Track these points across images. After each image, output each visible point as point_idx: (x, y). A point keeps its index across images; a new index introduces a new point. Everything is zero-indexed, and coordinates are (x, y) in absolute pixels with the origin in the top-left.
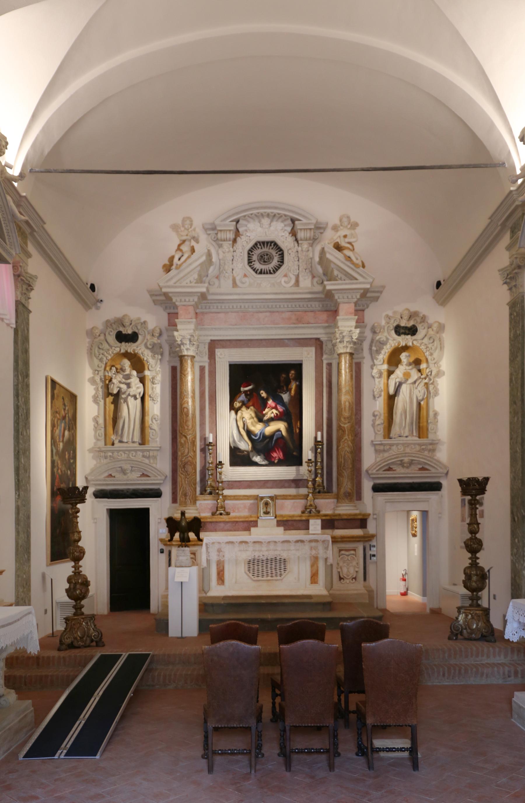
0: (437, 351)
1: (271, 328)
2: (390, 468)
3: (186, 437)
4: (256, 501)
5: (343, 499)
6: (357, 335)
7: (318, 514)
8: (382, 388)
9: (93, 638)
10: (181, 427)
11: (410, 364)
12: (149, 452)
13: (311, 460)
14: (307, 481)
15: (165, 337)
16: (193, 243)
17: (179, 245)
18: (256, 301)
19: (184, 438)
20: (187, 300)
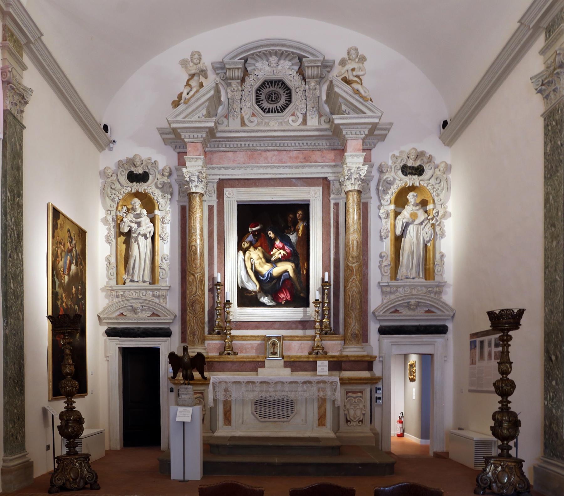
0: (444, 191)
1: (279, 166)
2: (396, 310)
3: (194, 276)
4: (263, 342)
5: (351, 341)
6: (365, 172)
7: (325, 355)
8: (389, 229)
9: (87, 480)
10: (190, 266)
11: (417, 205)
12: (159, 291)
13: (318, 300)
14: (315, 322)
15: (174, 176)
16: (202, 79)
17: (188, 81)
18: (265, 139)
19: (192, 277)
20: (196, 136)
